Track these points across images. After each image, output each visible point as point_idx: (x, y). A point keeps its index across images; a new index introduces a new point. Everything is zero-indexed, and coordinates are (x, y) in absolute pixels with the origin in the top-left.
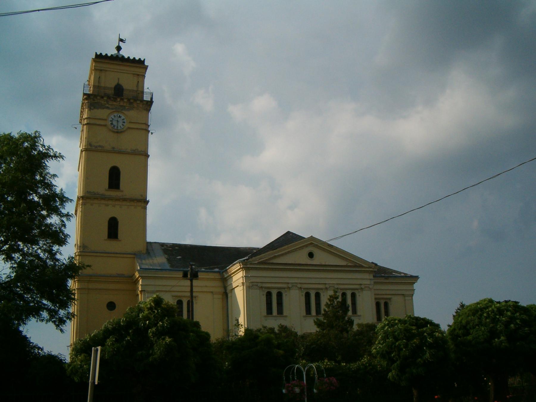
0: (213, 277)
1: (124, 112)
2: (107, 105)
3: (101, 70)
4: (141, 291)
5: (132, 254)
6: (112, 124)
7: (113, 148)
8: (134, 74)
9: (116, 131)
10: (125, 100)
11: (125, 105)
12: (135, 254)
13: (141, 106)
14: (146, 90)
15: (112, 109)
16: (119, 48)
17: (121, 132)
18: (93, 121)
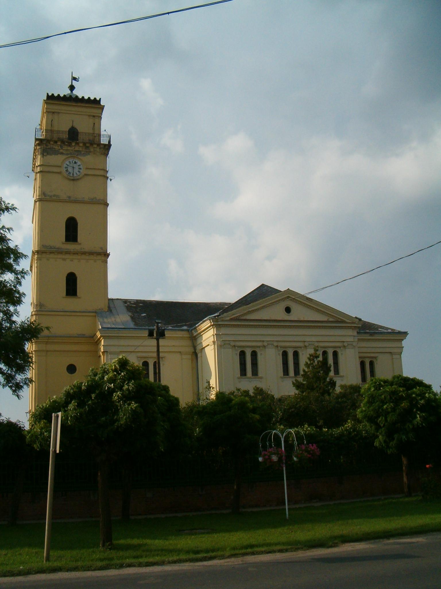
0: (181, 336)
1: (80, 157)
2: (61, 151)
3: (53, 113)
4: (103, 353)
5: (93, 312)
6: (67, 171)
7: (70, 197)
8: (89, 116)
9: (72, 178)
10: (81, 145)
11: (81, 149)
12: (96, 312)
13: (98, 150)
14: (102, 133)
15: (67, 154)
16: (72, 88)
17: (81, 179)
18: (46, 169)
